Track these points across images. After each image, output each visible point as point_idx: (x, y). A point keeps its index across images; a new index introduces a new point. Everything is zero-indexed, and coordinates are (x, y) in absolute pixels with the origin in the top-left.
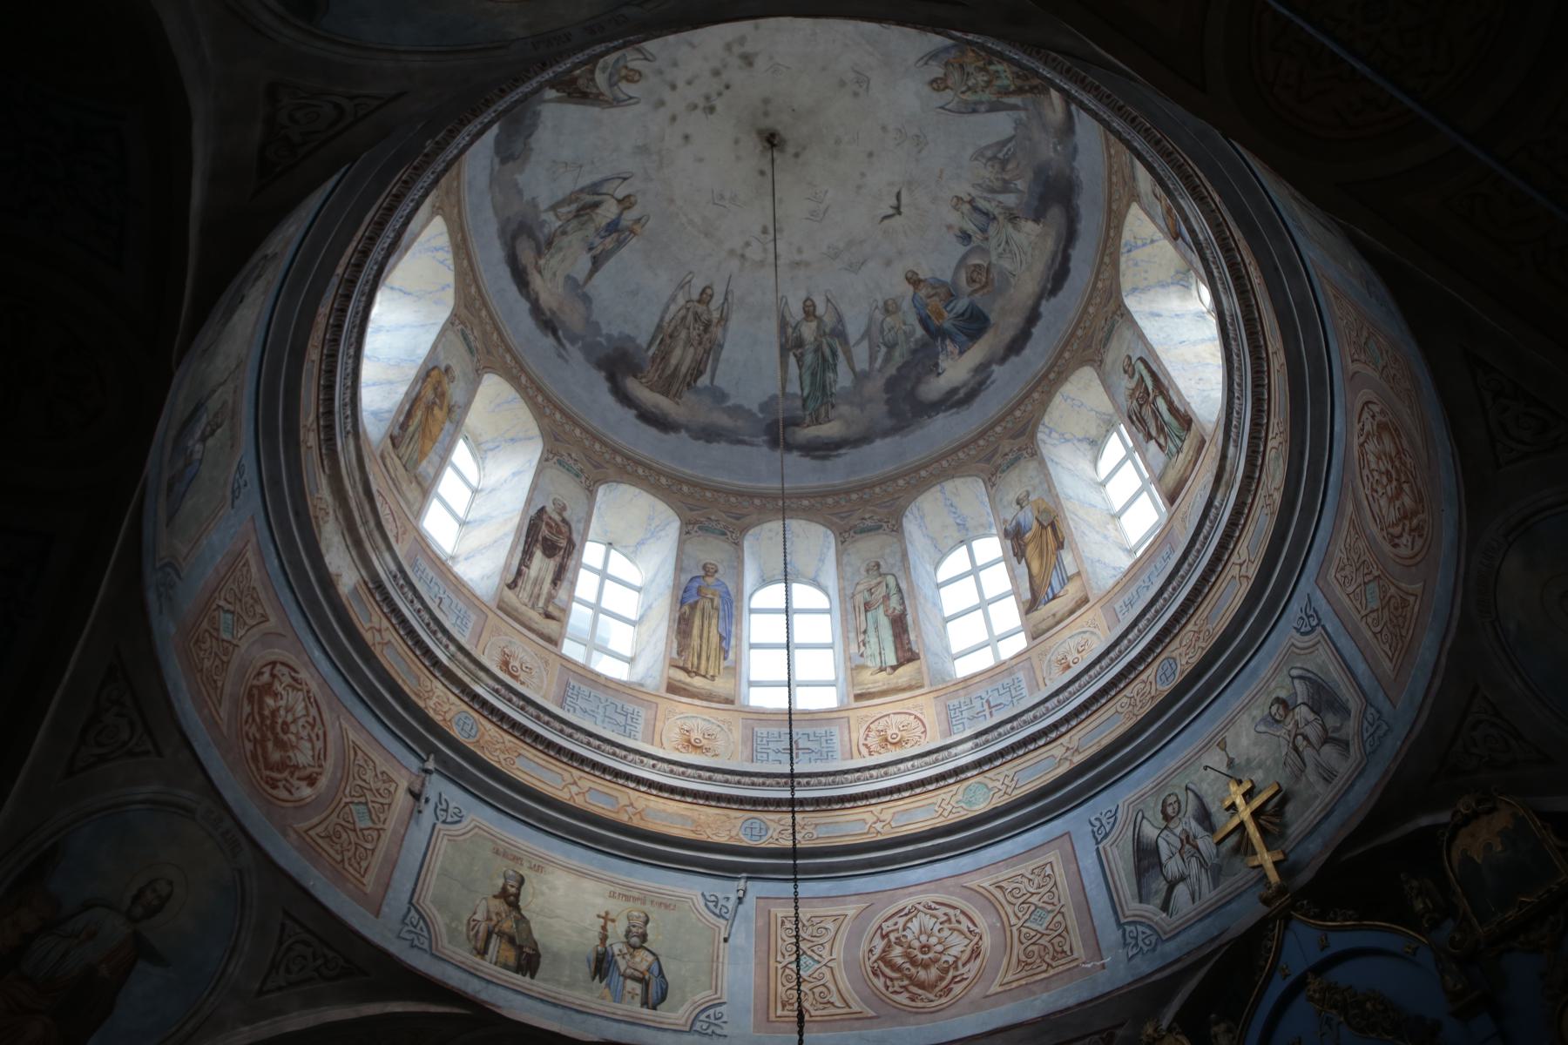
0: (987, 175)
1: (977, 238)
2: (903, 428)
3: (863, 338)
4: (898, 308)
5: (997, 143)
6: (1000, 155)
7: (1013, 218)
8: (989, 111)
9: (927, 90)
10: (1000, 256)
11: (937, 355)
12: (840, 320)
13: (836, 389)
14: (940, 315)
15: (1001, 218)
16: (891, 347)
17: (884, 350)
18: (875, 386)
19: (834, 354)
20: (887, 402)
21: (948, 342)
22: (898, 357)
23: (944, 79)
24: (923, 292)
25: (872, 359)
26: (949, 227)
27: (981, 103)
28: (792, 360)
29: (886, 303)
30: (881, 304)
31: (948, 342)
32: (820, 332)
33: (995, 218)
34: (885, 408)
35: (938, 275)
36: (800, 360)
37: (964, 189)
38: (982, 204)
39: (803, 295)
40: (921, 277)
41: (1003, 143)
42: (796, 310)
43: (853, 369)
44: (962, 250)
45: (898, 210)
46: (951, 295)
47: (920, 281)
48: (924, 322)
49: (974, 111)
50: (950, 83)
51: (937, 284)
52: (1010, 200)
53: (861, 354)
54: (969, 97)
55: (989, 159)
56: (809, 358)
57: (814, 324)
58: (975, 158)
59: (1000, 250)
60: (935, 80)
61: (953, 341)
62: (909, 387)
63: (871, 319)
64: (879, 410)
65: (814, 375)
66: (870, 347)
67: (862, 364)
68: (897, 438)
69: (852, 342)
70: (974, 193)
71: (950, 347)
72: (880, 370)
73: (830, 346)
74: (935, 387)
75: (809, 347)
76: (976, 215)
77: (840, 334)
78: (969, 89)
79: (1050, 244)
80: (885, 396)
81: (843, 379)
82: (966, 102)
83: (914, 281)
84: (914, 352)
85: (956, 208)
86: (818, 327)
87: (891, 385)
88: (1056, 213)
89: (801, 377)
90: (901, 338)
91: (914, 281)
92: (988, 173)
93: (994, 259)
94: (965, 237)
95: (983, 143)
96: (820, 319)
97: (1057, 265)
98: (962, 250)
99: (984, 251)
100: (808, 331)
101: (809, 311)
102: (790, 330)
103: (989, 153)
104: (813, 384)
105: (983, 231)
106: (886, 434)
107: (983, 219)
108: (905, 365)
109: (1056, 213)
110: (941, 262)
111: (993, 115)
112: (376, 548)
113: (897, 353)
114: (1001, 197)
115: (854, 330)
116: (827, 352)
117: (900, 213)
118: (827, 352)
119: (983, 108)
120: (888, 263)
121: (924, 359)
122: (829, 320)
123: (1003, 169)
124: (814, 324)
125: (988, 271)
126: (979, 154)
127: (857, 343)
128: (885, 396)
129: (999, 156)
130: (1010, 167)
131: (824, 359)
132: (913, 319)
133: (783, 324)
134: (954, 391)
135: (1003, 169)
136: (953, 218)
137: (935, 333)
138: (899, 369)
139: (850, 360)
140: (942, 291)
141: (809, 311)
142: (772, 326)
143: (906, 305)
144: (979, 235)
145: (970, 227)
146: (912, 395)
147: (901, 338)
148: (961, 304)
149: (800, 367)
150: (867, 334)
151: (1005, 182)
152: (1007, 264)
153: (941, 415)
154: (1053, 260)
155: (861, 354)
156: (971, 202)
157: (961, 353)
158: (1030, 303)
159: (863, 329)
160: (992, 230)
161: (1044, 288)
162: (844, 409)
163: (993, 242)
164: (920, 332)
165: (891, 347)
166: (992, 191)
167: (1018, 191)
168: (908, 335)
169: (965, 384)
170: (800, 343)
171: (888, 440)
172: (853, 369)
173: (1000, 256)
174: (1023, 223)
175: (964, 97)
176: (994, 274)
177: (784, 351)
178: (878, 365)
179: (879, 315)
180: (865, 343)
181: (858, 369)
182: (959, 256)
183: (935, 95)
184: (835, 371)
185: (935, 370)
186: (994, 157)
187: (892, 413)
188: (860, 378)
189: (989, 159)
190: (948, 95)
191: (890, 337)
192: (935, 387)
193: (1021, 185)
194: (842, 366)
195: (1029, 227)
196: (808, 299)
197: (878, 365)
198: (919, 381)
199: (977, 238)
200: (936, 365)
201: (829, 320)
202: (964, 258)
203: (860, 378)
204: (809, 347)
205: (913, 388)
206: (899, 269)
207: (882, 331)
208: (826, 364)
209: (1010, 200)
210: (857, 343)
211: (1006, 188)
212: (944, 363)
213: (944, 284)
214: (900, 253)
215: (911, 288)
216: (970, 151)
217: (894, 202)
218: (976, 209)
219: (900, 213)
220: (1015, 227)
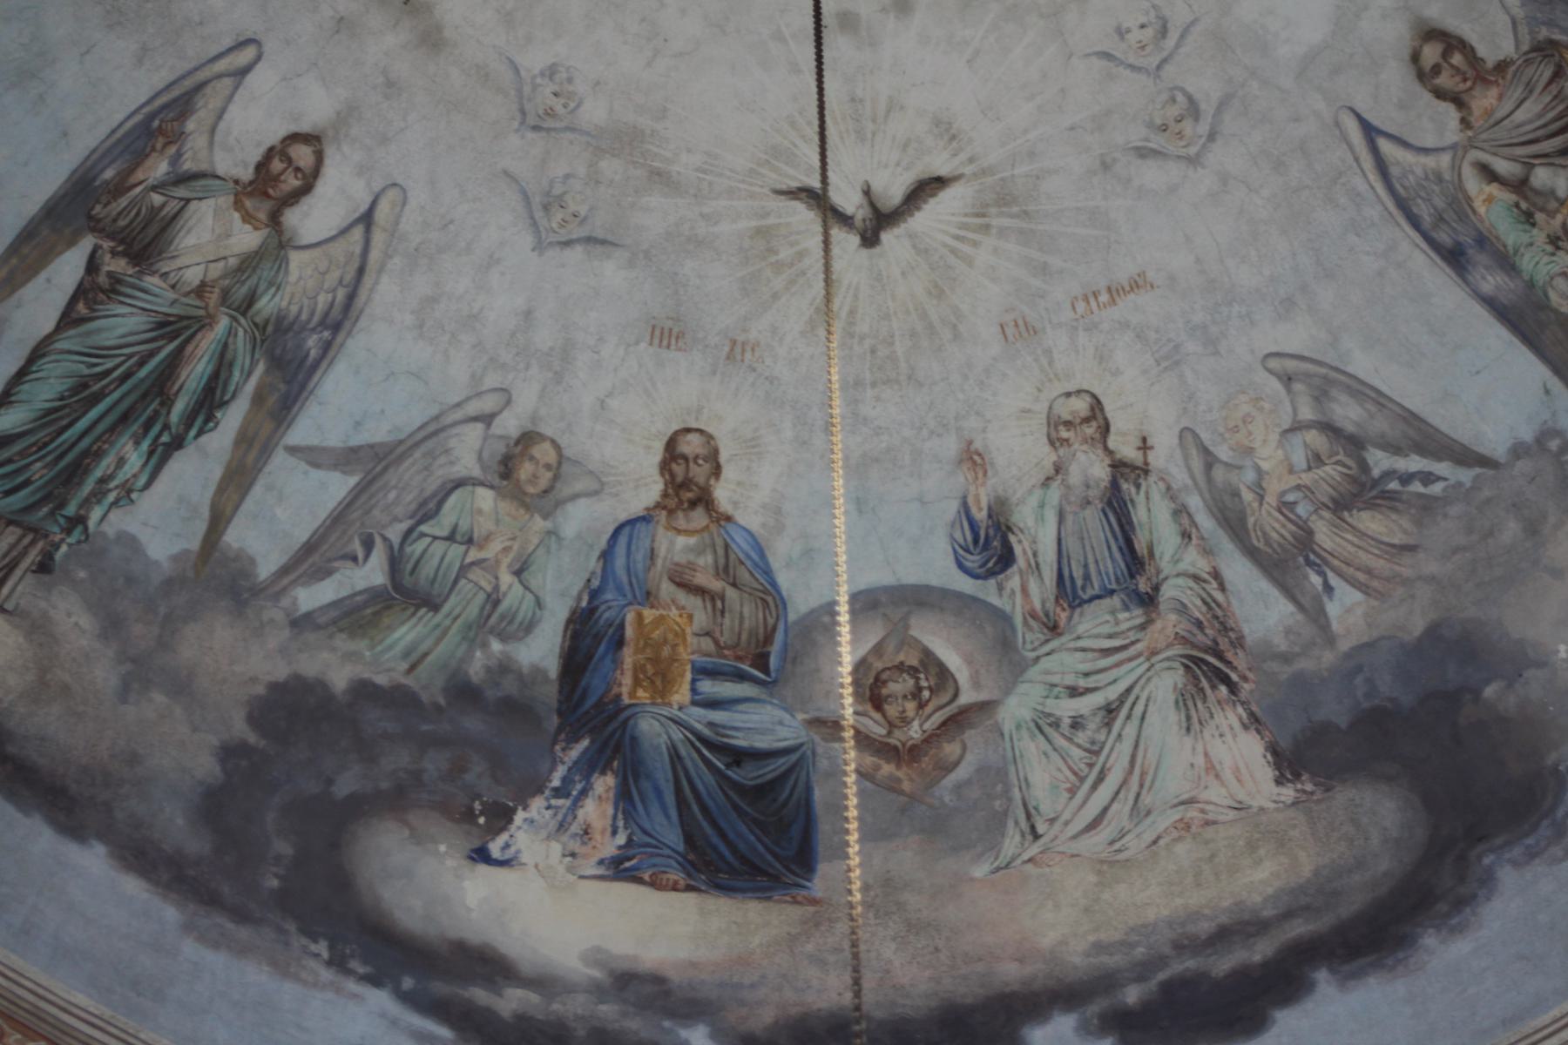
0: (1269, 455)
1: (1024, 591)
2: (209, 899)
3: (345, 458)
4: (546, 501)
5: (1411, 418)
6: (1379, 461)
7: (1210, 665)
8: (1492, 304)
9: (1393, 34)
10: (1044, 724)
11: (532, 787)
12: (339, 320)
13: (109, 522)
14: (659, 676)
15: (1168, 623)
16: (406, 593)
17: (373, 573)
18: (237, 659)
19: (210, 402)
20: (230, 753)
21: (604, 784)
22: (400, 650)
23: (1482, 73)
24: (676, 545)
25: (311, 558)
26: (973, 459)
27: (1506, 262)
28: (68, 268)
29: (528, 439)
30: (510, 424)
31: (604, 784)
32: (239, 287)
33: (1148, 601)
34: (206, 767)
35: (781, 553)
36: (92, 294)
37: (1146, 412)
38: (1154, 519)
39: (316, 106)
40: (722, 494)
41: (1425, 438)
42: (243, 130)
43: (218, 521)
44: (935, 564)
45: (878, 222)
46: (765, 652)
47: (704, 500)
48: (588, 639)
49: (1455, 258)
50: (1483, 100)
51: (745, 571)
52: (1263, 611)
53: (291, 504)
54: (1492, 208)
55: (1329, 429)
56: (122, 324)
57: (247, 238)
58: (1291, 372)
59: (1067, 708)
60: (1451, 43)
61: (625, 797)
62: (347, 784)
63: (433, 432)
64: (181, 751)
65: (83, 393)
66: (338, 518)
67: (271, 527)
68: (171, 914)
69: (302, 431)
70: (1165, 455)
71: (597, 809)
72: (301, 623)
73: (223, 364)
74: (434, 882)
75: (157, 294)
76: (1094, 521)
77: (292, 362)
78: (1520, 186)
79: (1259, 880)
80: (240, 728)
81: (158, 515)
82: (1460, 204)
83: (688, 477)
84: (464, 693)
85: (1057, 430)
86: (249, 263)
87: (292, 710)
88: (1375, 823)
89: (38, 353)
90: (465, 602)
91: (688, 477)
92: (1277, 460)
93: (1016, 708)
94: (990, 544)
95: (1362, 365)
96: (279, 244)
97: (1223, 964)
98: (935, 564)
99: (1009, 659)
100: (210, 237)
101: (279, 181)
102: (159, 168)
103: (1348, 413)
104: (53, 417)
105: (1070, 593)
106: (141, 856)
107: (1109, 564)
108: (398, 699)
109: (1375, 823)
110: (840, 532)
111: (1496, 337)
112: (450, 566)
113: (407, 632)
114: (1239, 570)
115: (341, 406)
116: (195, 373)
117: (870, 239)
118: (195, 373)
119: (1492, 282)
120: (667, 334)
121: (491, 746)
122: (301, 285)
123: (1340, 506)
124: (247, 238)
125: (958, 721)
126: (1315, 378)
127: (313, 456)
128: (240, 728)
129: (1373, 461)
130: (1371, 522)
131: (162, 386)
132: (558, 588)
133: (162, 123)
134: (491, 966)
135: (1340, 506)
136: (1019, 453)
137: (584, 707)
138: (364, 691)
139: (239, 478)
140: (744, 611)
141: (279, 181)
142: (124, 87)
143: (586, 519)
144: (1041, 591)
145: (1037, 534)
146: (330, 825)
147: (465, 602)
148: (763, 723)
149: (68, 319)
150: (373, 463)
151: (1305, 539)
152: (1042, 773)
153: (381, 999)
154: (1223, 936)
155: (291, 504)
156: (1119, 467)
157: (619, 869)
158: (1011, 973)
159: (377, 433)
160: (1099, 622)
161: (1105, 982)
162: (71, 615)
163: (1064, 663)
164: (541, 650)
165: (406, 593)
166: (1234, 523)
167: (1317, 616)
168: (494, 619)
169: (544, 983)
170: (145, 243)
171: (133, 886)
172: (218, 521)
173: (1044, 724)
174: (1230, 718)
175: (1473, 184)
176: (970, 754)
177: (74, 207)
178: (312, 597)
179: (466, 451)
180: (339, 486)
181: (236, 536)
182: (910, 575)
183: (1397, 75)
184: (160, 456)
185: (483, 826)
186: (1355, 444)
187: (213, 806)
188: (216, 577)
189: (1329, 429)
190: (1436, 124)
191: (434, 556)
192: (434, 882)
193: (1347, 608)
194: (196, 470)
195: (1238, 757)
196: (312, 139)
197: (312, 597)
198: (396, 800)
199: (1024, 591)
200: (501, 817)
201: (301, 285)
202: (919, 598)
203: (216, 577)
204: (157, 294)
205: (359, 808)
206: (683, 391)
207: (427, 510)
208: (149, 401)
209: (1263, 611)
210: (313, 456)
211: (1287, 562)
212: (529, 833)
213: (770, 596)
214: (737, 351)
215: (653, 490)
216: (1297, 336)
217: (893, 190)
218: (1117, 507)
219: (870, 239)
220: (1186, 700)
